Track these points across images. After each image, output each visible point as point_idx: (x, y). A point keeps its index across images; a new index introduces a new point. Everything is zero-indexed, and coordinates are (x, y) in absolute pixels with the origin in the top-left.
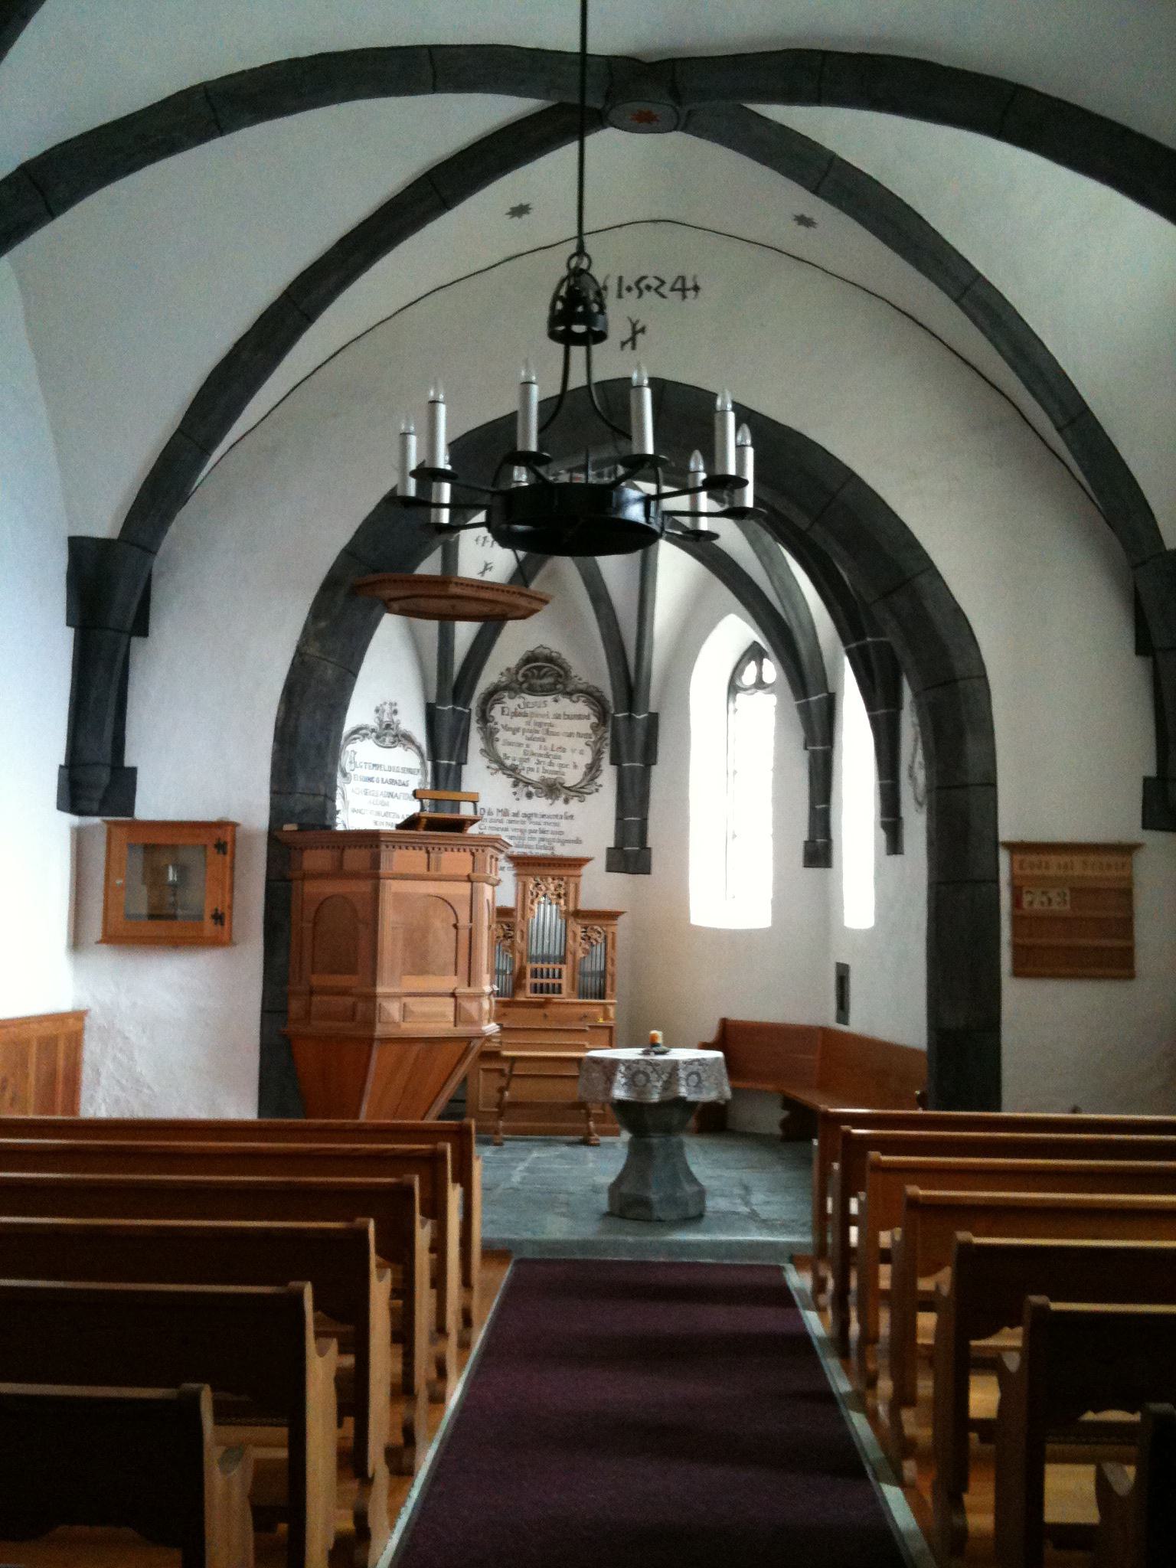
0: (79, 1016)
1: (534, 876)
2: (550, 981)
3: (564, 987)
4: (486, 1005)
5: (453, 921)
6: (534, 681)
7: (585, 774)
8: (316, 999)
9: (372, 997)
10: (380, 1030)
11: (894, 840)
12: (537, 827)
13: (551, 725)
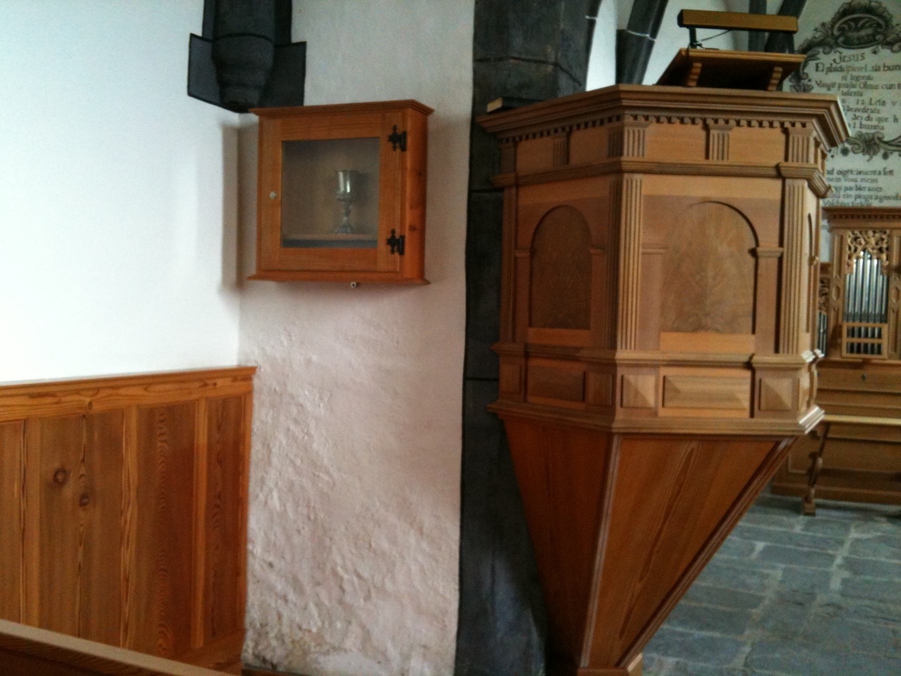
0: (243, 375)
1: (852, 229)
2: (869, 341)
3: (885, 348)
4: (805, 382)
5: (753, 245)
6: (850, 34)
8: (534, 363)
9: (610, 367)
10: (621, 420)
12: (852, 184)
13: (869, 78)
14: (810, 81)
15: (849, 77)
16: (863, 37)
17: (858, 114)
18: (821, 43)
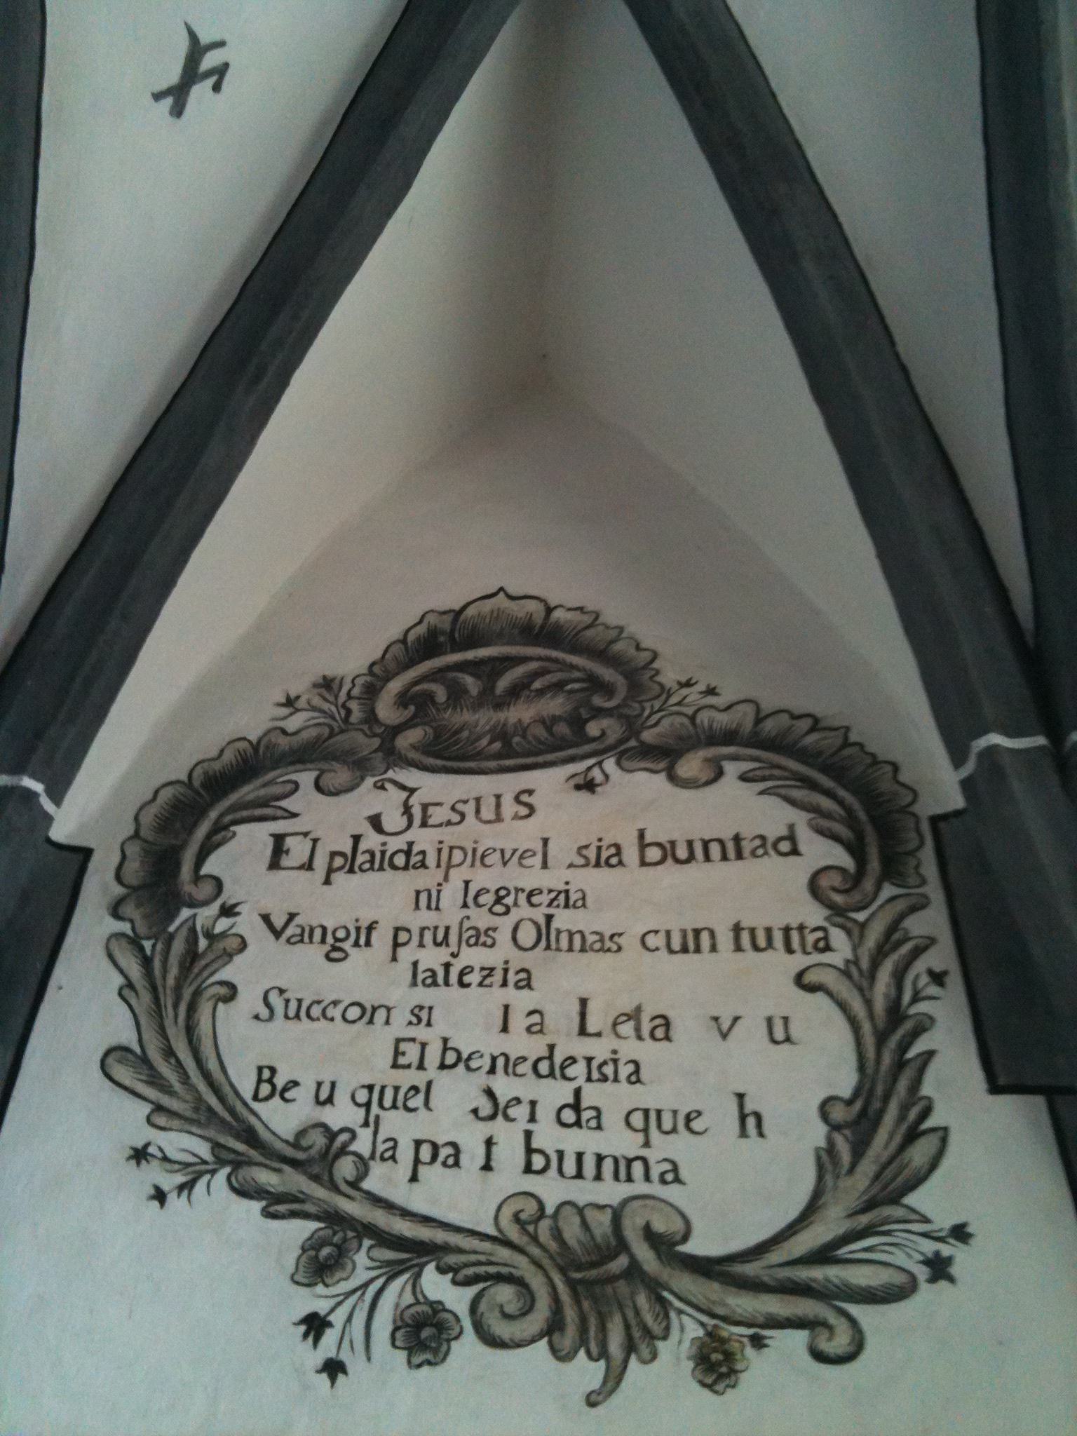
7: (826, 1160)
11: (891, 1137)
13: (564, 898)
14: (228, 911)
15: (451, 894)
16: (522, 729)
17: (504, 1087)
18: (306, 753)
